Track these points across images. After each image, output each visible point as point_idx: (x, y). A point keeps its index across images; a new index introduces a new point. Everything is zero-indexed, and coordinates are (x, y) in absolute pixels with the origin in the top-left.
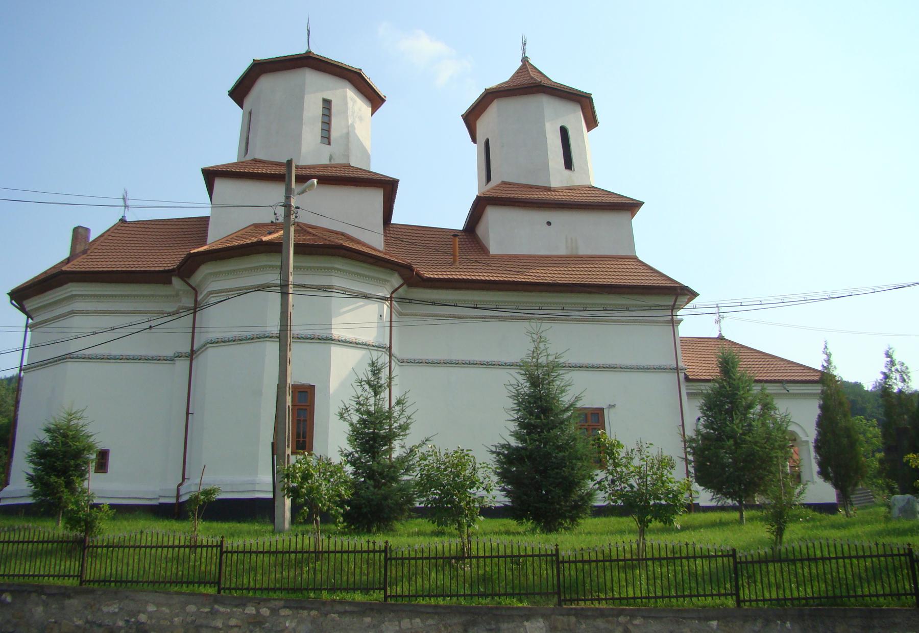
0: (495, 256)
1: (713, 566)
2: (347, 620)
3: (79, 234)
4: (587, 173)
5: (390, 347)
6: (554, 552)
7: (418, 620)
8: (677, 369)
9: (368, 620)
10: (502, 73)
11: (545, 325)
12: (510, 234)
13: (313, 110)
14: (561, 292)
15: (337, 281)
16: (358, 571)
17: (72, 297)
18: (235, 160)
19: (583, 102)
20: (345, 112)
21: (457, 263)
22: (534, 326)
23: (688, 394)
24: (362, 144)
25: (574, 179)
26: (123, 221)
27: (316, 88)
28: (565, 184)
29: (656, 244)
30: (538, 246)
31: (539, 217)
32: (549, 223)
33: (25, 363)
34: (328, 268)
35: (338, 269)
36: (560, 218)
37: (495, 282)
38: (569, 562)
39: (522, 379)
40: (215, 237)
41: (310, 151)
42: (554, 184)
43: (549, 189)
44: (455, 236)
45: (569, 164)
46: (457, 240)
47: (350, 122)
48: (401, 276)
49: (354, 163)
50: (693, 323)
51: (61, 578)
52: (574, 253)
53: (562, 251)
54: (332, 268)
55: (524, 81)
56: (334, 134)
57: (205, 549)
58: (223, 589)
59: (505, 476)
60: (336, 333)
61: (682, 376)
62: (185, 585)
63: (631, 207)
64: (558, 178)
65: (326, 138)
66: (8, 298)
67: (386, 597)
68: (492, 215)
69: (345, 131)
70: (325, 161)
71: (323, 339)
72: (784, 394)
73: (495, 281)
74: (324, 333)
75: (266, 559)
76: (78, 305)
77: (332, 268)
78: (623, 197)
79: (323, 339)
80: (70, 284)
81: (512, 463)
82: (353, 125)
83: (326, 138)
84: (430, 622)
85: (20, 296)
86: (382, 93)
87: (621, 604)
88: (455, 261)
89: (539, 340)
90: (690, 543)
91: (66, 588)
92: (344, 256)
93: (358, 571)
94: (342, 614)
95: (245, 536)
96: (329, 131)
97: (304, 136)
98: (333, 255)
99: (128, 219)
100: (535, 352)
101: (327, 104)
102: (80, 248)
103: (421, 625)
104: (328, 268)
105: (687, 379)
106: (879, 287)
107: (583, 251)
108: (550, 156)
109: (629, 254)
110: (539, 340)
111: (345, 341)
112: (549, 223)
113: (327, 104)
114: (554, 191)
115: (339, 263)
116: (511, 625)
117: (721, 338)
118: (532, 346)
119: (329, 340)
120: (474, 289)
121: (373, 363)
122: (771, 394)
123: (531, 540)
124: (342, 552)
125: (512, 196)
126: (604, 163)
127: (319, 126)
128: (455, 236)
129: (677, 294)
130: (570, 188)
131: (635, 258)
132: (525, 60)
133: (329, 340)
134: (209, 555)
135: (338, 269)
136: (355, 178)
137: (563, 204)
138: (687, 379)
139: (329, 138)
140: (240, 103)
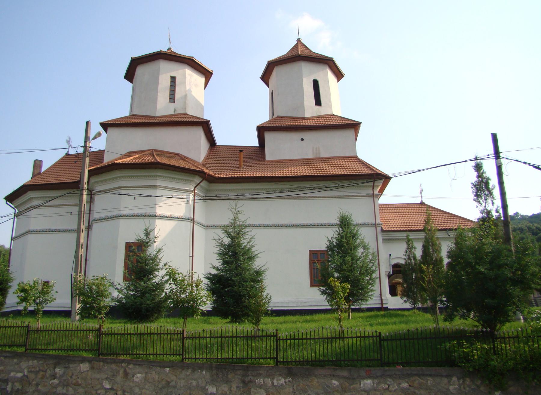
0: (268, 162)
1: (367, 342)
2: (7, 360)
3: (37, 164)
4: (331, 107)
5: (193, 219)
6: (275, 334)
7: (35, 361)
8: (375, 225)
9: (15, 360)
10: (282, 50)
11: (241, 203)
12: (281, 148)
13: (164, 82)
14: (303, 181)
15: (159, 183)
16: (309, 351)
17: (31, 199)
18: (128, 115)
19: (328, 62)
20: (185, 82)
21: (242, 167)
22: (233, 203)
23: (383, 239)
24: (197, 101)
25: (322, 111)
26: (67, 154)
27: (166, 70)
28: (315, 115)
29: (370, 150)
30: (305, 153)
31: (295, 136)
32: (302, 140)
33: (13, 236)
34: (154, 176)
35: (160, 176)
36: (308, 136)
37: (237, 178)
38: (283, 339)
39: (222, 235)
40: (107, 159)
41: (163, 108)
42: (307, 115)
43: (304, 119)
44: (241, 151)
45: (318, 102)
46: (242, 153)
47: (188, 88)
48: (201, 177)
49: (190, 112)
50: (391, 195)
51: (66, 351)
52: (318, 156)
53: (310, 156)
54: (157, 176)
55: (294, 53)
56: (178, 96)
57: (156, 335)
58: (185, 358)
59: (213, 291)
60: (159, 211)
61: (379, 229)
62: (7, 347)
63: (354, 126)
64: (310, 110)
65: (172, 99)
66: (5, 200)
67: (26, 350)
68: (268, 137)
69: (184, 94)
70: (172, 113)
71: (150, 216)
72: (447, 238)
73: (248, 177)
74: (149, 212)
75: (191, 341)
76: (35, 203)
77: (157, 176)
78: (349, 120)
79: (150, 216)
80: (29, 192)
81: (219, 284)
82: (190, 91)
83: (172, 99)
84: (41, 362)
85: (10, 198)
86: (210, 68)
87: (288, 365)
88: (240, 166)
89: (236, 213)
90: (378, 331)
91: (173, 361)
92: (162, 168)
93: (309, 351)
94: (6, 357)
95: (59, 323)
96: (174, 95)
97: (159, 99)
98: (156, 168)
99: (70, 153)
100: (235, 219)
101: (173, 79)
102: (37, 172)
103: (37, 364)
104: (154, 176)
105: (383, 231)
106: (397, 173)
107: (323, 155)
108: (305, 98)
109: (352, 154)
110: (236, 213)
111: (164, 217)
112: (302, 140)
113: (173, 79)
114: (307, 120)
115: (159, 173)
116: (75, 365)
117: (422, 203)
118: (232, 217)
119: (154, 216)
120: (248, 182)
121: (145, 230)
122: (412, 239)
123: (221, 325)
124: (66, 330)
125: (277, 125)
126: (339, 101)
127: (168, 92)
128: (241, 151)
129: (378, 179)
130: (318, 117)
131: (356, 157)
132: (299, 40)
133: (154, 216)
134: (285, 346)
135: (160, 176)
136: (191, 121)
137: (307, 127)
138: (383, 231)
139: (174, 99)
140: (131, 81)
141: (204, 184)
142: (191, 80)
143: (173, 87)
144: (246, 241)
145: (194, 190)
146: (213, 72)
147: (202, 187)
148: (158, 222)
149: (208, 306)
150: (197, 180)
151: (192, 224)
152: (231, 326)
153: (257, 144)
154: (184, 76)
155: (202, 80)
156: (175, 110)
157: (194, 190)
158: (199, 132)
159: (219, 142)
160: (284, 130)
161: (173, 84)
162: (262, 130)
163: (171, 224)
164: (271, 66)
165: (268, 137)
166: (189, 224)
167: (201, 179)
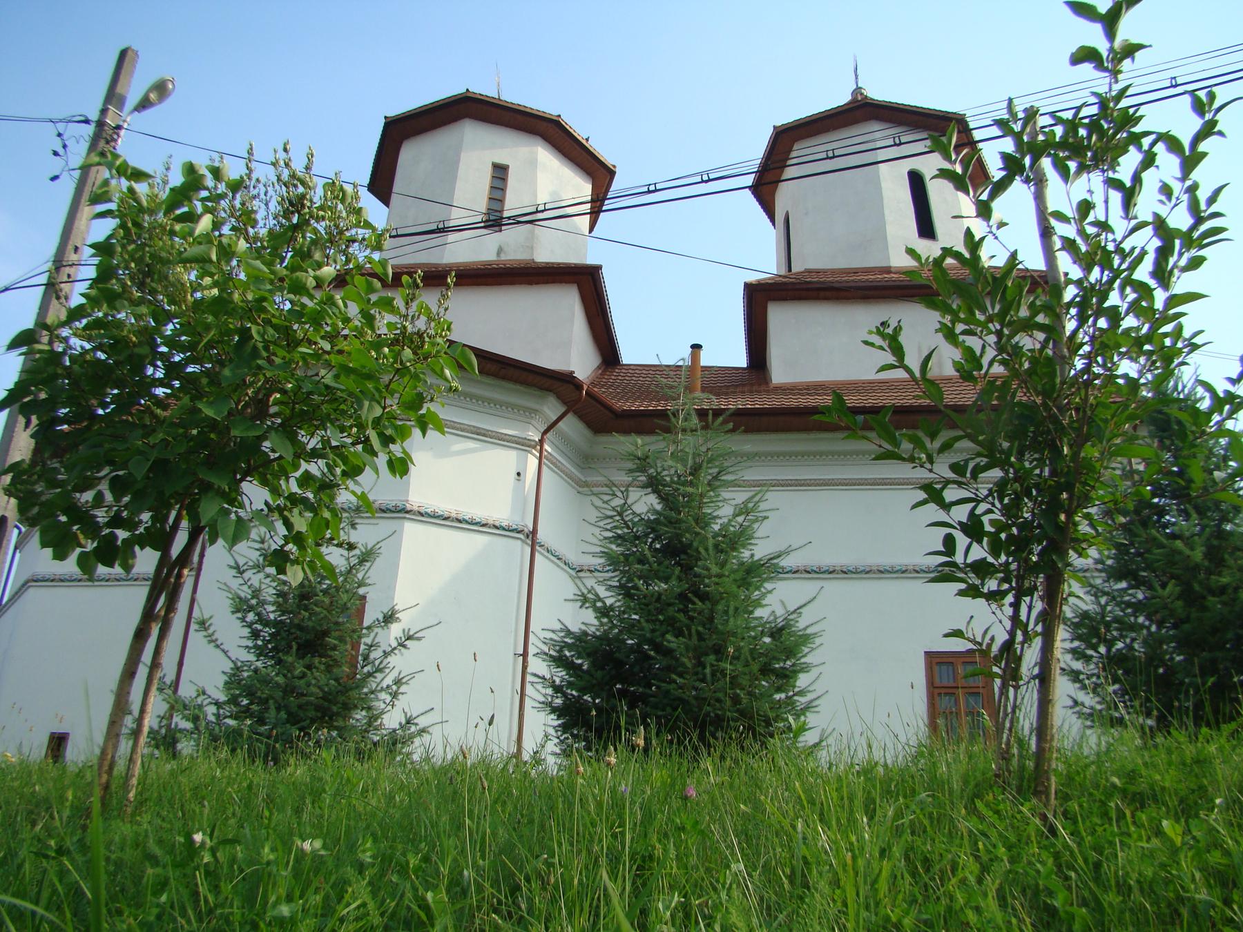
48: (561, 398)
68: (779, 317)
101: (500, 172)
108: (889, 216)
111: (434, 516)
113: (500, 172)
119: (401, 512)
133: (401, 512)
141: (571, 426)
142: (548, 179)
143: (497, 195)
144: (726, 511)
145: (541, 441)
146: (617, 170)
147: (564, 438)
148: (412, 531)
149: (79, 550)
150: (551, 408)
151: (528, 550)
152: (949, 235)
153: (740, 359)
154: (533, 163)
155: (583, 188)
156: (500, 251)
157: (541, 441)
158: (567, 304)
159: (628, 355)
160: (826, 299)
161: (498, 184)
162: (759, 298)
163: (464, 547)
164: (785, 140)
165: (779, 317)
166: (518, 549)
167: (563, 409)
